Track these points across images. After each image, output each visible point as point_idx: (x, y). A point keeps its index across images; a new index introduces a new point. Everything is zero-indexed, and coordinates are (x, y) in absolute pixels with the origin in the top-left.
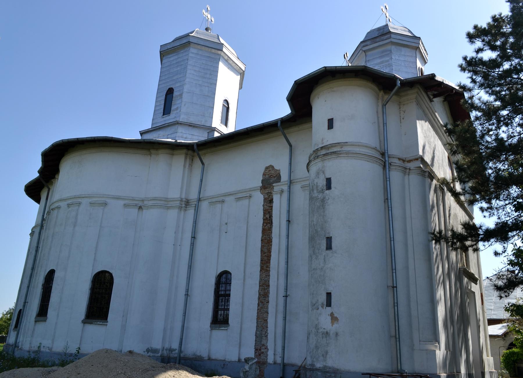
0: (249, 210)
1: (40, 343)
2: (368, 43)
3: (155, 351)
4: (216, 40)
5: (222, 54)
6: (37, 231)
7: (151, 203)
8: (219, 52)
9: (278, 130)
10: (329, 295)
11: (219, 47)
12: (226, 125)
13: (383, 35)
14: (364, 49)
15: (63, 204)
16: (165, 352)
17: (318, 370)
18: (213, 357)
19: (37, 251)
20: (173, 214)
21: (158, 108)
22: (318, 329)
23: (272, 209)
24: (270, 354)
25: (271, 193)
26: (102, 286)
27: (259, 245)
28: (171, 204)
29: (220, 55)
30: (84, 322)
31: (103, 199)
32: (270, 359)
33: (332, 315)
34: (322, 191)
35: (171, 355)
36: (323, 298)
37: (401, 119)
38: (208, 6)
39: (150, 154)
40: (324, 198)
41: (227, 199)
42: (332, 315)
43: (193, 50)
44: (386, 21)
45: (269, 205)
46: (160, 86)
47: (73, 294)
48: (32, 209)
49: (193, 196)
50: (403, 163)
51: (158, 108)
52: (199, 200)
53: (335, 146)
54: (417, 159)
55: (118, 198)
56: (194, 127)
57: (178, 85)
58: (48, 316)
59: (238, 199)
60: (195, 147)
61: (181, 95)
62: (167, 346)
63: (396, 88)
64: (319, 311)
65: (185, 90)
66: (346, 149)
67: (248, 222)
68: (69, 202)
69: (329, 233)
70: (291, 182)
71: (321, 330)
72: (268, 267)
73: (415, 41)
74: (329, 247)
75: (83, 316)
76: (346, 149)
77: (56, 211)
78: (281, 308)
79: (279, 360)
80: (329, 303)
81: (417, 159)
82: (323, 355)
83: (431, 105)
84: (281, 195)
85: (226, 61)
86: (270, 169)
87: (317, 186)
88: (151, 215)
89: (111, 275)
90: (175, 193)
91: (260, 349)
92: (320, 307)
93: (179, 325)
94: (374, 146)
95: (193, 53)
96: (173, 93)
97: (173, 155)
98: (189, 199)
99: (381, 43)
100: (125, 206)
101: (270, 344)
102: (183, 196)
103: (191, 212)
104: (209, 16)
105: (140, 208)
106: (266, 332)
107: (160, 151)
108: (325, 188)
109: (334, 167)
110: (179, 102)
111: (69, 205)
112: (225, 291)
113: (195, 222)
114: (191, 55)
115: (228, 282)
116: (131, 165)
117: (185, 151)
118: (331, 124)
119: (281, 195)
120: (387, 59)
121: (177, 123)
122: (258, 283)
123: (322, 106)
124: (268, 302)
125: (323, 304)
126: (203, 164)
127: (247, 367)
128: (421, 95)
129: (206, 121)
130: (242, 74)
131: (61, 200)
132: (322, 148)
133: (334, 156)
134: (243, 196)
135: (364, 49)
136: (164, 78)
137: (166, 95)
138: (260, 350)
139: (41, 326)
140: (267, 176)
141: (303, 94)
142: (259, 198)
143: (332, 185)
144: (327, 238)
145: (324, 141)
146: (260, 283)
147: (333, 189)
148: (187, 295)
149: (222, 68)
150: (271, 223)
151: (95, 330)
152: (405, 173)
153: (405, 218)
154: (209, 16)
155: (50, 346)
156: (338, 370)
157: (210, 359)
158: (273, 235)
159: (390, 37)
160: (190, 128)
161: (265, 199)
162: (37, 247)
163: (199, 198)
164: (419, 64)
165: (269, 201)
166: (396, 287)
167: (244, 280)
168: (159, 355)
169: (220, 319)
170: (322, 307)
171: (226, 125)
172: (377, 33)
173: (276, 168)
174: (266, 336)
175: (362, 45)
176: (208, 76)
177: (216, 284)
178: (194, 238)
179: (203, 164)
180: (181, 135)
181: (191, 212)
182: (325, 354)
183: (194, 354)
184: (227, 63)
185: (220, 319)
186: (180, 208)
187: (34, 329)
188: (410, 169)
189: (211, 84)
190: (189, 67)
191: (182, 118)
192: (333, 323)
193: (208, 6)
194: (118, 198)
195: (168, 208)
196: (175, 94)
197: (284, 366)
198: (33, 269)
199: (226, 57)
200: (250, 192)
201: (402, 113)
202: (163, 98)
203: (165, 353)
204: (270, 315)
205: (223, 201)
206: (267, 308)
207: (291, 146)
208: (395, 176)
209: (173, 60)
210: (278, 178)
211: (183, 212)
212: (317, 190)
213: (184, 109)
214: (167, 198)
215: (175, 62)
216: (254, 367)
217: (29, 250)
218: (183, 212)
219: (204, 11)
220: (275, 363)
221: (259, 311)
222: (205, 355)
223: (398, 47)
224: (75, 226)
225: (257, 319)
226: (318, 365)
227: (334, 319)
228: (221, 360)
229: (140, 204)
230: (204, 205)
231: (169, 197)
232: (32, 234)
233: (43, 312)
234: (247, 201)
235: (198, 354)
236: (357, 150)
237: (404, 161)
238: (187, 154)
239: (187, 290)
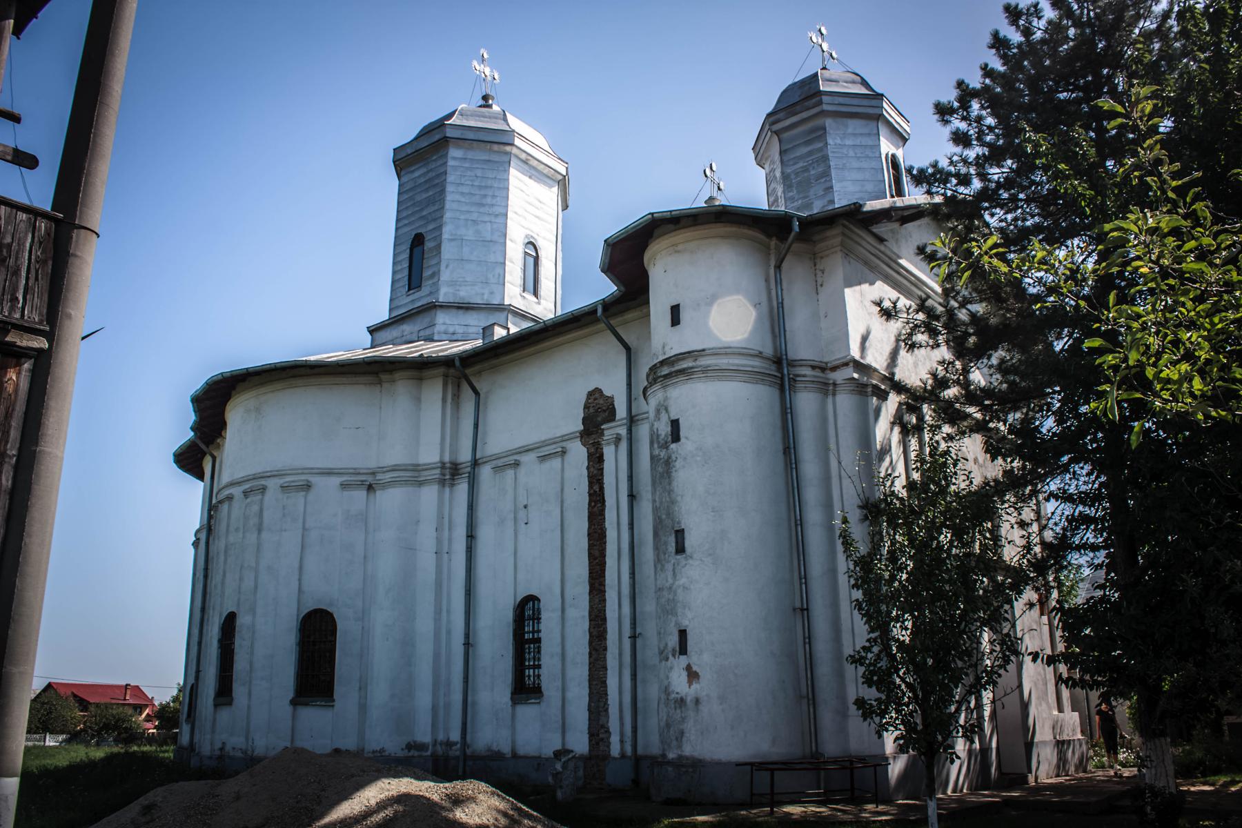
0: (562, 478)
1: (224, 743)
2: (781, 115)
3: (421, 747)
4: (501, 126)
5: (515, 151)
6: (203, 536)
7: (388, 477)
8: (508, 148)
9: (597, 320)
10: (683, 634)
14: (776, 127)
15: (236, 491)
16: (439, 748)
17: (670, 763)
18: (521, 752)
19: (206, 577)
20: (429, 494)
21: (398, 276)
22: (669, 695)
23: (602, 474)
24: (615, 739)
25: (599, 443)
26: (317, 634)
27: (584, 543)
28: (426, 475)
29: (510, 154)
30: (294, 703)
31: (303, 477)
32: (615, 750)
33: (688, 668)
35: (451, 753)
36: (673, 640)
37: (817, 287)
38: (482, 51)
39: (380, 383)
40: (669, 457)
41: (524, 459)
42: (688, 668)
44: (823, 60)
45: (597, 466)
46: (400, 232)
48: (193, 492)
49: (465, 456)
50: (821, 375)
51: (398, 276)
52: (475, 463)
53: (683, 359)
54: (846, 364)
55: (329, 473)
56: (467, 309)
57: (431, 227)
59: (543, 458)
60: (457, 363)
62: (441, 737)
63: (793, 234)
64: (669, 663)
65: (445, 236)
66: (703, 362)
67: (562, 502)
68: (246, 486)
69: (679, 523)
70: (632, 420)
71: (673, 696)
72: (603, 584)
73: (874, 102)
74: (680, 549)
76: (703, 362)
77: (225, 507)
78: (627, 658)
79: (629, 750)
80: (683, 650)
81: (846, 364)
83: (882, 248)
84: (617, 446)
85: (525, 162)
86: (597, 395)
87: (658, 436)
88: (391, 500)
89: (331, 615)
90: (430, 455)
91: (598, 731)
92: (671, 657)
93: (457, 697)
94: (756, 346)
95: (454, 158)
97: (421, 379)
99: (805, 115)
100: (344, 486)
101: (613, 724)
103: (462, 488)
104: (487, 71)
106: (606, 703)
107: (397, 375)
110: (434, 262)
112: (533, 632)
113: (471, 507)
114: (451, 163)
115: (537, 618)
116: (347, 403)
117: (442, 370)
118: (675, 315)
119: (617, 446)
120: (820, 145)
121: (432, 307)
122: (587, 614)
123: (669, 273)
124: (605, 649)
125: (674, 650)
126: (477, 393)
127: (559, 767)
128: (854, 237)
129: (492, 293)
130: (563, 184)
131: (232, 484)
132: (663, 363)
133: (682, 378)
134: (553, 451)
135: (776, 127)
136: (404, 214)
139: (224, 714)
140: (592, 410)
141: (629, 256)
142: (578, 453)
143: (682, 434)
144: (677, 532)
145: (667, 348)
146: (590, 615)
147: (683, 440)
148: (467, 644)
149: (517, 179)
150: (603, 502)
151: (312, 716)
152: (826, 394)
153: (827, 478)
154: (487, 71)
156: (700, 761)
157: (515, 755)
159: (820, 103)
160: (461, 312)
161: (590, 456)
162: (206, 569)
164: (887, 147)
165: (596, 459)
166: (807, 609)
167: (563, 610)
168: (429, 753)
169: (525, 688)
170: (674, 656)
173: (607, 393)
175: (772, 119)
176: (489, 200)
177: (515, 621)
178: (471, 537)
179: (477, 393)
180: (442, 328)
181: (462, 488)
183: (489, 750)
184: (526, 167)
185: (525, 688)
186: (442, 482)
187: (215, 720)
188: (835, 384)
189: (497, 216)
190: (449, 188)
191: (444, 294)
192: (690, 683)
193: (482, 51)
194: (329, 473)
195: (421, 484)
196: (429, 245)
197: (637, 760)
198: (203, 609)
200: (564, 444)
201: (819, 273)
204: (609, 672)
205: (517, 464)
207: (628, 349)
208: (806, 402)
209: (419, 177)
210: (610, 413)
211: (447, 490)
213: (445, 276)
215: (422, 180)
216: (571, 765)
217: (194, 574)
218: (447, 490)
219: (475, 63)
222: (506, 749)
223: (840, 120)
224: (260, 531)
225: (590, 681)
226: (671, 755)
227: (692, 675)
229: (370, 479)
230: (485, 472)
231: (421, 461)
232: (196, 544)
233: (224, 692)
234: (559, 460)
235: (495, 748)
236: (723, 362)
237: (823, 369)
238: (446, 376)
239: (467, 636)
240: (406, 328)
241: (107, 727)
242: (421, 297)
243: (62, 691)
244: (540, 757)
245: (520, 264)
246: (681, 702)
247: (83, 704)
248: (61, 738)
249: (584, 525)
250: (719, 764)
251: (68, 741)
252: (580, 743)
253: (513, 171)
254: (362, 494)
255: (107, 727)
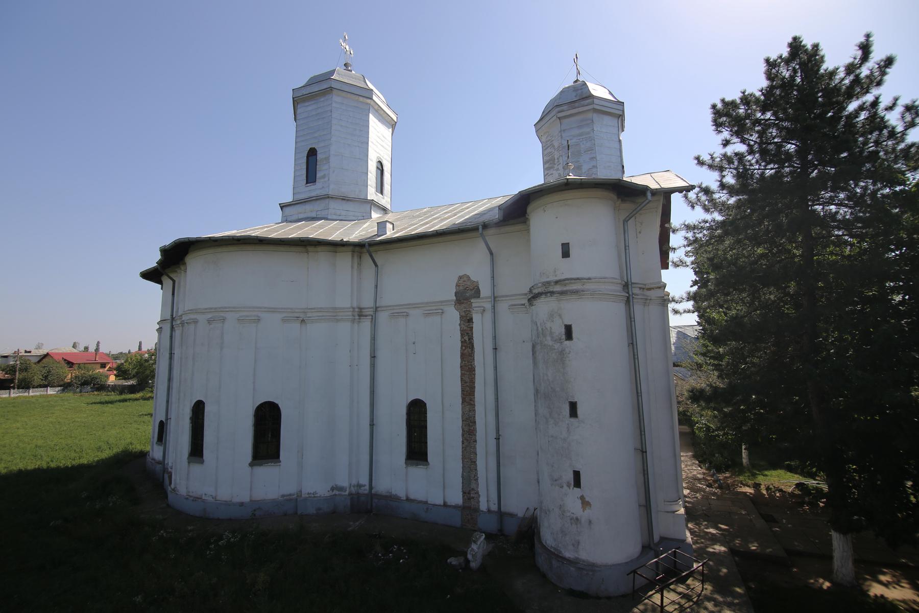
2: (565, 107)
3: (341, 489)
5: (372, 103)
8: (369, 101)
11: (368, 94)
12: (382, 193)
13: (584, 99)
18: (412, 497)
25: (470, 311)
26: (267, 419)
27: (458, 372)
30: (251, 465)
32: (483, 507)
33: (582, 498)
34: (559, 341)
35: (360, 491)
36: (570, 477)
42: (582, 498)
43: (336, 98)
47: (231, 431)
52: (376, 309)
55: (273, 310)
57: (322, 144)
58: (204, 457)
59: (427, 315)
61: (327, 159)
62: (354, 482)
66: (589, 286)
70: (495, 299)
71: (568, 514)
75: (249, 459)
76: (589, 286)
79: (494, 508)
80: (577, 482)
82: (573, 545)
85: (377, 111)
87: (551, 333)
90: (344, 300)
91: (469, 492)
92: (565, 487)
93: (367, 457)
96: (316, 155)
98: (362, 306)
99: (581, 109)
100: (284, 320)
102: (355, 305)
103: (366, 324)
105: (303, 321)
106: (476, 475)
108: (564, 337)
109: (574, 311)
111: (209, 321)
113: (373, 339)
114: (334, 105)
126: (376, 265)
132: (557, 282)
134: (433, 309)
137: (308, 157)
138: (469, 493)
142: (453, 316)
149: (373, 120)
151: (266, 471)
155: (214, 494)
157: (408, 499)
158: (476, 363)
161: (461, 317)
163: (376, 308)
168: (347, 493)
169: (417, 452)
170: (569, 486)
171: (382, 193)
172: (574, 94)
174: (477, 480)
178: (373, 357)
179: (376, 265)
181: (366, 324)
182: (576, 545)
185: (417, 452)
186: (353, 321)
192: (584, 509)
195: (338, 321)
199: (376, 107)
202: (305, 160)
203: (353, 490)
204: (478, 457)
206: (475, 448)
210: (477, 293)
212: (552, 337)
214: (335, 308)
220: (489, 511)
221: (464, 449)
222: (402, 495)
226: (568, 554)
227: (585, 503)
228: (420, 502)
229: (302, 315)
230: (383, 317)
232: (160, 330)
235: (394, 493)
240: (308, 209)
241: (85, 383)
242: (315, 190)
243: (56, 357)
244: (426, 503)
245: (374, 173)
246: (577, 520)
247: (70, 364)
248: (57, 389)
249: (458, 361)
250: (607, 566)
251: (63, 390)
252: (456, 497)
253: (371, 116)
254: (297, 325)
255: (85, 383)
